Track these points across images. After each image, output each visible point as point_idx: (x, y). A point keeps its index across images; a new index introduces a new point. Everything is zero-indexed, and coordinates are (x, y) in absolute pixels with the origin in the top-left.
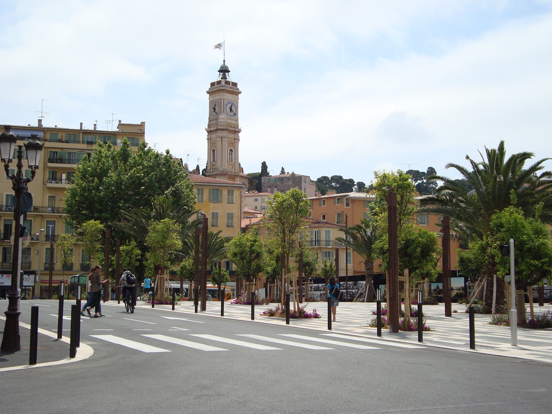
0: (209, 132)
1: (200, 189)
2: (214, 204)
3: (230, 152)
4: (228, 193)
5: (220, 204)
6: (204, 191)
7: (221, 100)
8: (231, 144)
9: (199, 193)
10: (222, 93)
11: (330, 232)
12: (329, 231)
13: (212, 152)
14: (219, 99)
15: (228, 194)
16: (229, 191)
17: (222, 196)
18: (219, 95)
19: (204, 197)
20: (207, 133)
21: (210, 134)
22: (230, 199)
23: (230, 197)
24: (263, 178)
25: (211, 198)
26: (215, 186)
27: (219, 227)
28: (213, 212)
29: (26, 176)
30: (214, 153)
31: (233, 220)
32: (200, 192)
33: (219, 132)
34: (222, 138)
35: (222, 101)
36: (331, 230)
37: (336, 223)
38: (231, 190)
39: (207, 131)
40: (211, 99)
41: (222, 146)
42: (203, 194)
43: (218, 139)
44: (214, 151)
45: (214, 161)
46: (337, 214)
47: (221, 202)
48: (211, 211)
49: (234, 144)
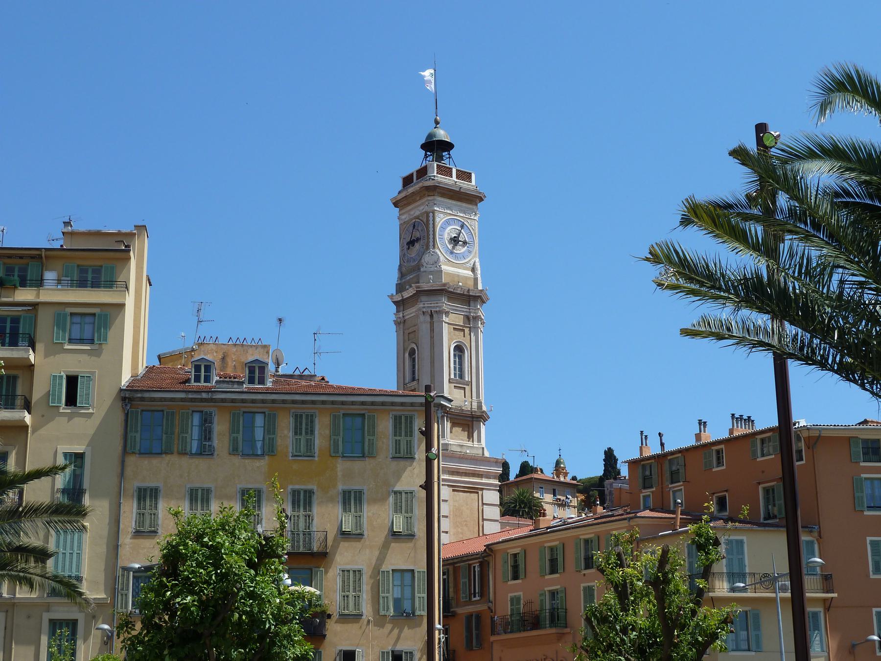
0: (401, 305)
1: (301, 416)
2: (348, 464)
3: (457, 353)
4: (395, 427)
5: (368, 463)
6: (317, 421)
7: (428, 217)
8: (457, 333)
9: (301, 429)
10: (430, 198)
11: (742, 546)
12: (740, 543)
13: (407, 355)
14: (422, 214)
15: (397, 431)
16: (397, 420)
17: (373, 434)
18: (423, 204)
19: (317, 442)
20: (394, 308)
21: (402, 308)
22: (403, 446)
23: (403, 440)
24: (607, 482)
25: (340, 443)
26: (353, 403)
27: (366, 536)
28: (346, 488)
29: (304, 547)
30: (414, 360)
31: (412, 511)
32: (301, 424)
33: (424, 298)
34: (431, 316)
35: (431, 219)
36: (745, 538)
37: (762, 520)
38: (406, 417)
39: (393, 302)
40: (403, 217)
41: (432, 337)
42: (312, 432)
43: (422, 318)
44: (412, 353)
45: (413, 379)
46: (764, 488)
47: (372, 455)
48: (341, 487)
49: (467, 330)
